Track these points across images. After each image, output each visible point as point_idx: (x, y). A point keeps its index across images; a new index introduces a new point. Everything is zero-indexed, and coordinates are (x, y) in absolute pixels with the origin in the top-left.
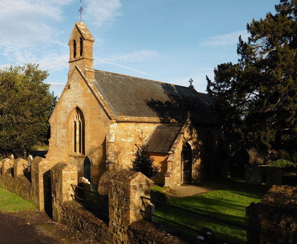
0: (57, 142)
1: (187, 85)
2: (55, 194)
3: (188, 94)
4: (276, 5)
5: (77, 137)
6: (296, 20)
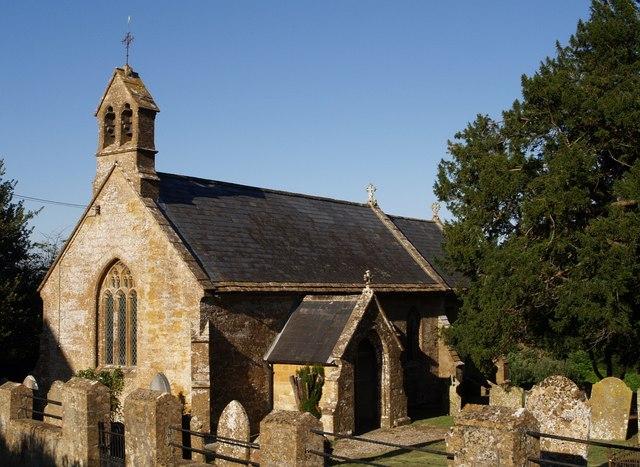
4: (524, 78)
5: (115, 328)
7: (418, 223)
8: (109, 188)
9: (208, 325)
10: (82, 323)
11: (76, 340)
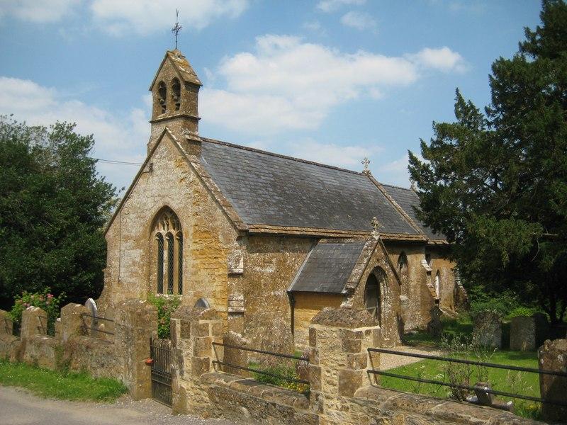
0: (122, 275)
1: (360, 169)
2: (181, 361)
3: (234, 162)
4: (520, 44)
5: (164, 264)
6: (563, 85)
7: (400, 190)
8: (162, 148)
9: (242, 260)
10: (138, 260)
11: (133, 274)
